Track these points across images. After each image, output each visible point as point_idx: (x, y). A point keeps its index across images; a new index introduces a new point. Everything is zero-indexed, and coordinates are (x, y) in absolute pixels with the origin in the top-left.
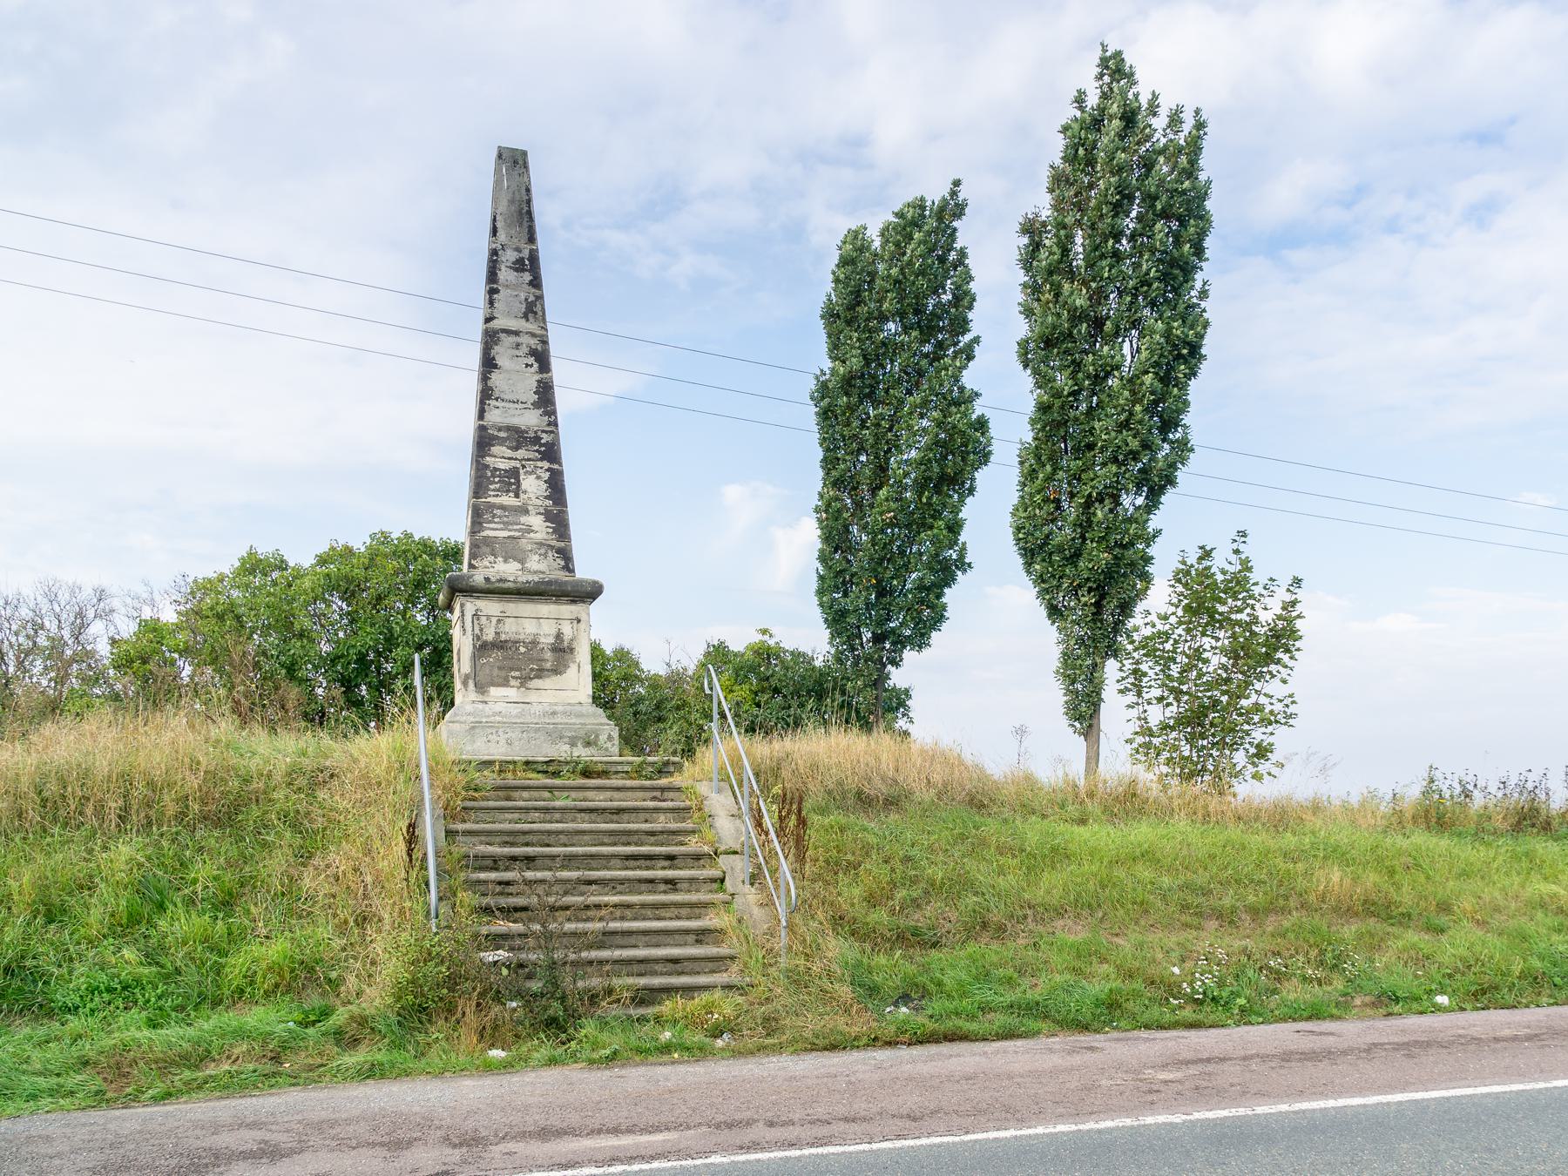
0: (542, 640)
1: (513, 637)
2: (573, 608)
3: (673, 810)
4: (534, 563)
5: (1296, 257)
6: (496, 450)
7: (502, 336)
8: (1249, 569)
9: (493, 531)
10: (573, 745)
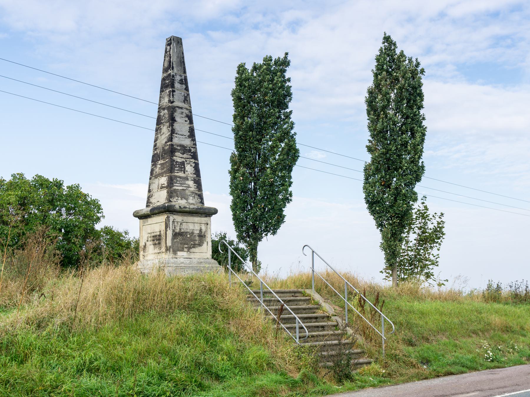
0: (195, 232)
4: (191, 200)
5: (215, 35)
6: (177, 154)
7: (177, 109)
8: (427, 209)
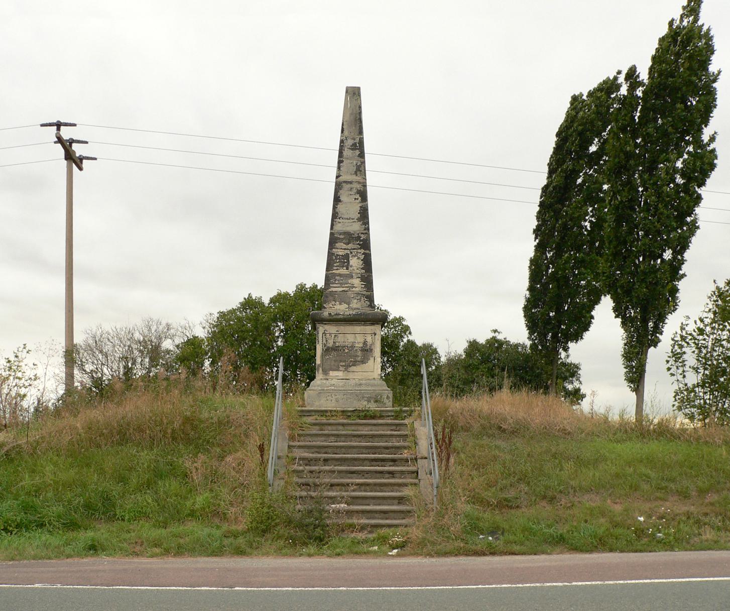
1: (342, 344)
2: (372, 327)
3: (400, 436)
4: (355, 304)
6: (338, 245)
7: (344, 184)
9: (336, 288)
10: (369, 401)
